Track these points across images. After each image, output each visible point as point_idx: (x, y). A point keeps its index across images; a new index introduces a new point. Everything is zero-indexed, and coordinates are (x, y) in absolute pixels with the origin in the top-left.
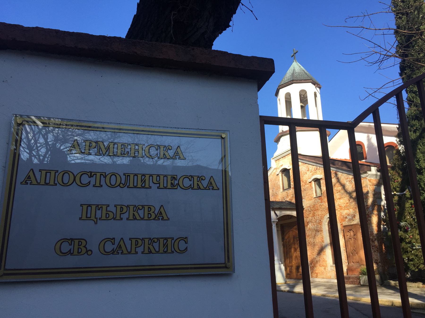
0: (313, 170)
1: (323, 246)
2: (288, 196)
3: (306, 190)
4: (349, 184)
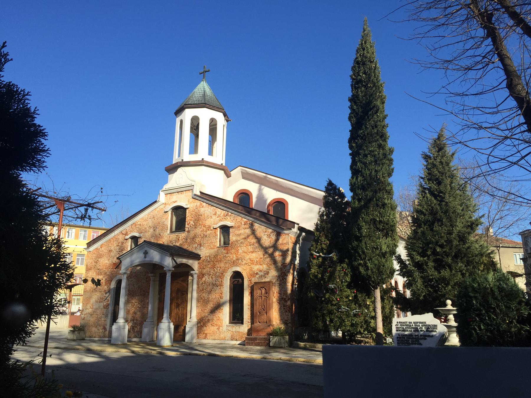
0: (222, 215)
1: (221, 303)
2: (179, 240)
3: (208, 236)
4: (266, 238)
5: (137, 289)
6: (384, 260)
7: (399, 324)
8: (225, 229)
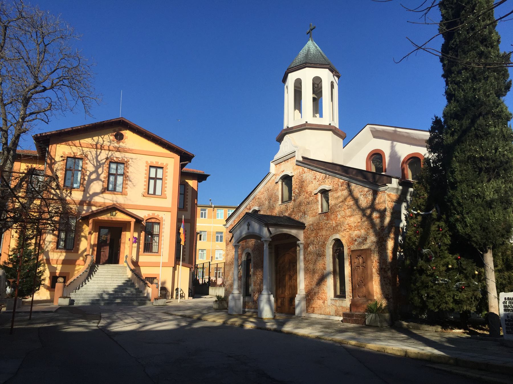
0: (321, 179)
2: (287, 210)
3: (310, 203)
6: (490, 212)
7: (508, 301)
8: (324, 193)
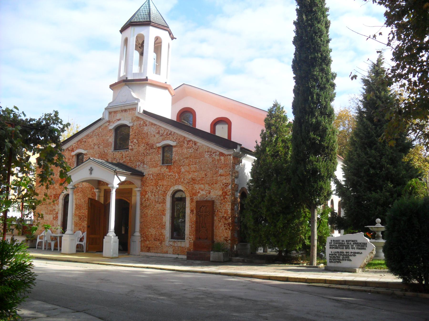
0: (165, 134)
2: (122, 157)
5: (84, 203)
